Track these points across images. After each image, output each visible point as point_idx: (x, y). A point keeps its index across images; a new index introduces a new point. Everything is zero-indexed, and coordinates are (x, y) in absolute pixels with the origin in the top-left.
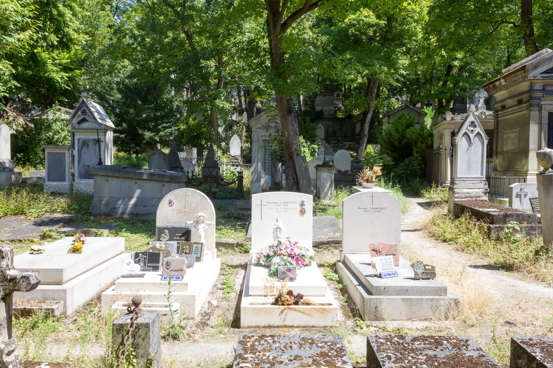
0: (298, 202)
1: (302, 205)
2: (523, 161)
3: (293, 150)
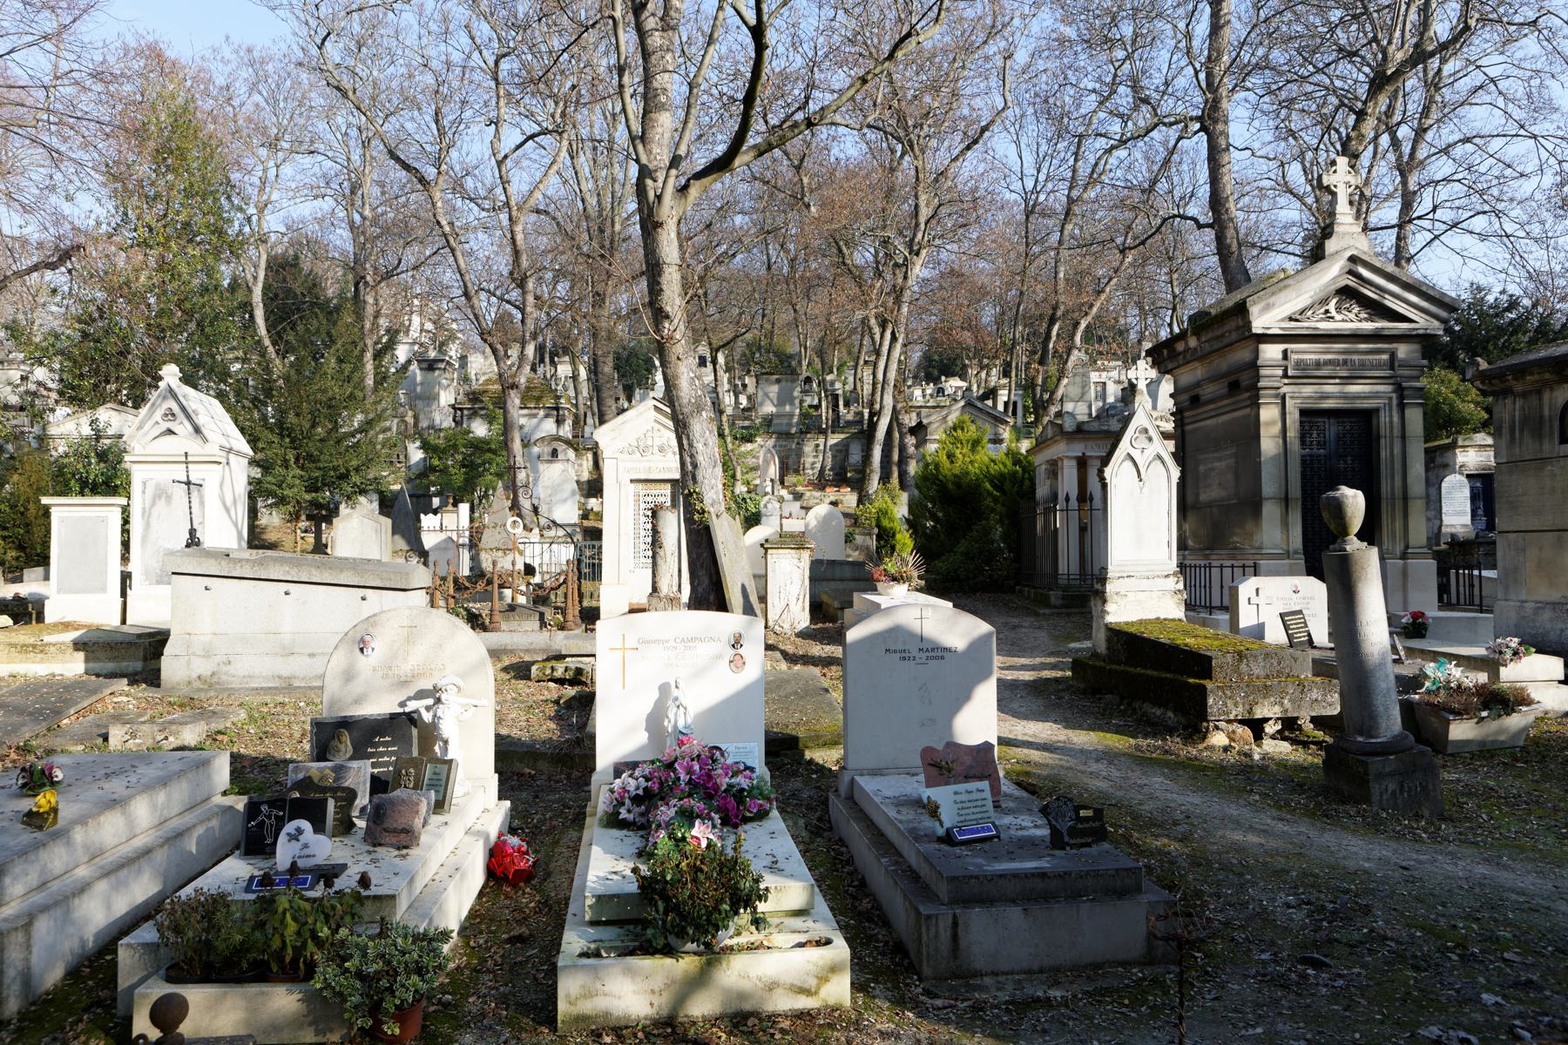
2: (1249, 526)
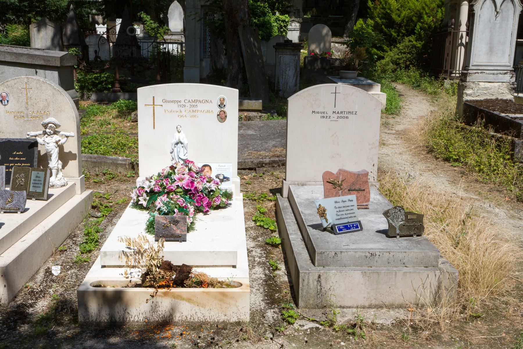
0: (217, 102)
1: (221, 105)
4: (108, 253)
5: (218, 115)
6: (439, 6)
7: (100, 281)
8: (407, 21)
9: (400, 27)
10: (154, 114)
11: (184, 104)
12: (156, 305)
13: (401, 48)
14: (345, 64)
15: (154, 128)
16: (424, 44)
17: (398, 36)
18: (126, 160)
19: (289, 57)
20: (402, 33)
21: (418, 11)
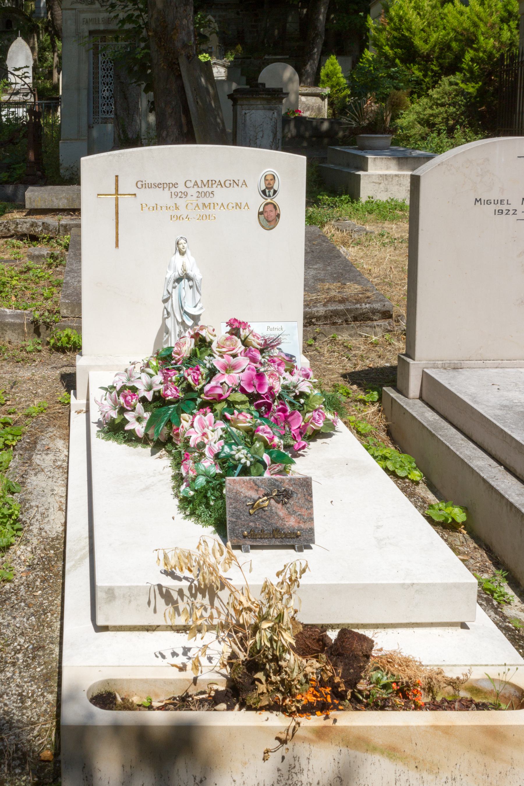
0: (257, 183)
1: (269, 191)
3: (178, 45)
4: (117, 592)
5: (260, 213)
6: (503, 20)
7: (108, 682)
8: (441, 49)
9: (427, 62)
10: (117, 213)
11: (184, 189)
12: (291, 767)
13: (435, 96)
14: (367, 122)
15: (117, 245)
16: (480, 87)
17: (425, 76)
18: (21, 316)
19: (261, 112)
20: (432, 71)
21: (465, 29)
